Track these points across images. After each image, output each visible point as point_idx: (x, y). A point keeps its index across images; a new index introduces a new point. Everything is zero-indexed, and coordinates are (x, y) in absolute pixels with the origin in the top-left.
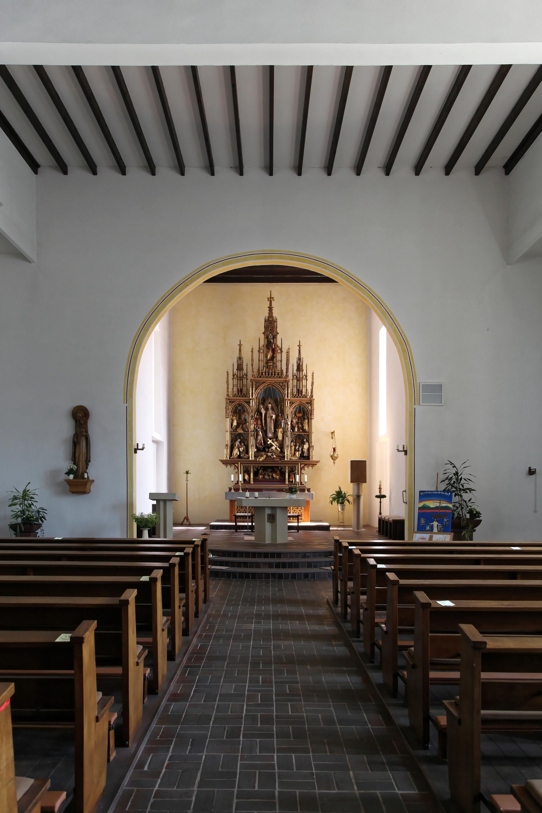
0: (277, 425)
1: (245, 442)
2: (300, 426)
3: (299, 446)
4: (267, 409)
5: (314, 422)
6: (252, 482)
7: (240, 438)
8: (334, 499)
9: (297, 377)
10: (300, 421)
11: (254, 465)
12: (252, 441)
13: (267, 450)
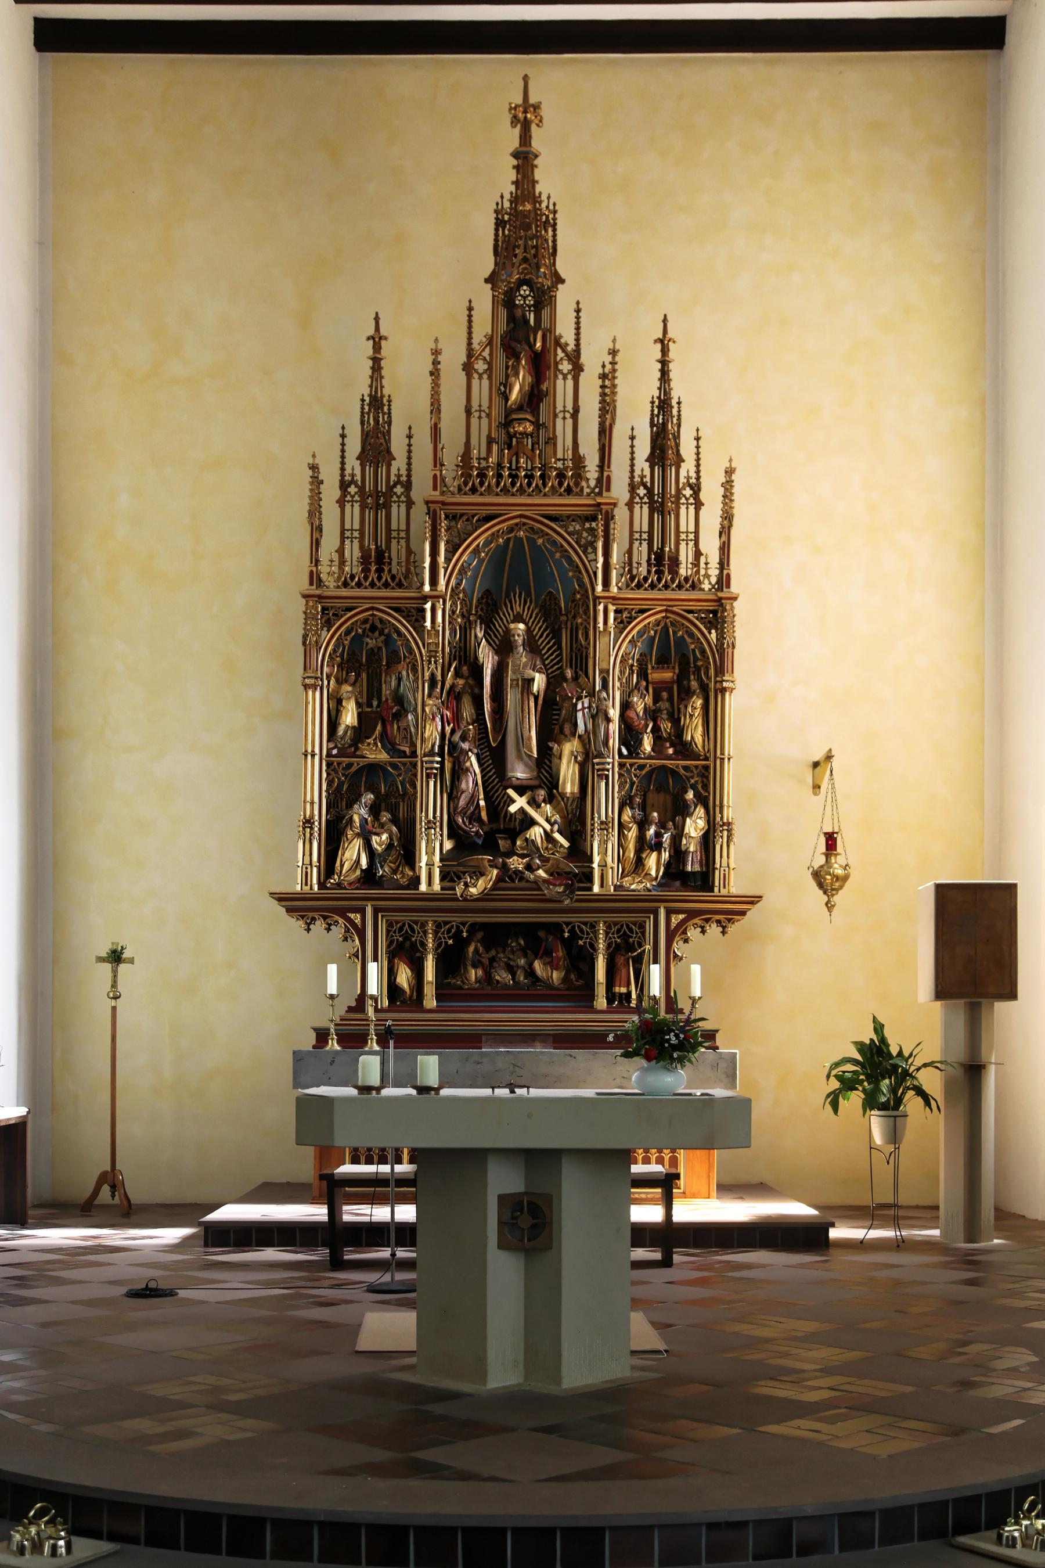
0: (554, 722)
1: (397, 808)
2: (666, 726)
3: (662, 825)
4: (504, 648)
5: (735, 706)
6: (430, 1001)
7: (371, 789)
8: (848, 1084)
9: (650, 491)
10: (664, 705)
11: (442, 918)
12: (431, 801)
13: (503, 844)
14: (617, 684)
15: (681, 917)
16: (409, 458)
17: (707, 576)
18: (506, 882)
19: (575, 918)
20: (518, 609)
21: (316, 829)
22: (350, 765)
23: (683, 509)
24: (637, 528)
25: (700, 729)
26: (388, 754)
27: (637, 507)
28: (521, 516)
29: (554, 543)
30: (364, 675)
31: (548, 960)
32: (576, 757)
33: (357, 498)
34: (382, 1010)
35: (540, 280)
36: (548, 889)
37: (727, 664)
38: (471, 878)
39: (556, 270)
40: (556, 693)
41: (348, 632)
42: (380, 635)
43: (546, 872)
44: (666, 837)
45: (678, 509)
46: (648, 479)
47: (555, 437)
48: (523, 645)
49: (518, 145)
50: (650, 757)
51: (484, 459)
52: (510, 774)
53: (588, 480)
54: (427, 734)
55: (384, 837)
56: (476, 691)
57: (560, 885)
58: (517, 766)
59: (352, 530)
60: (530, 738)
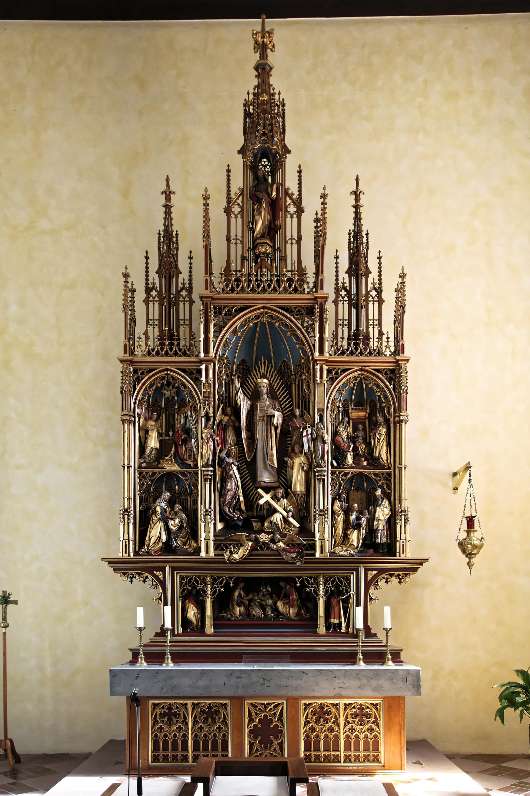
0: (288, 444)
1: (185, 501)
2: (362, 447)
3: (360, 512)
4: (254, 396)
5: (409, 432)
6: (210, 629)
7: (170, 489)
9: (349, 293)
10: (360, 434)
11: (216, 574)
12: (207, 498)
13: (256, 525)
14: (330, 419)
15: (374, 573)
16: (190, 272)
17: (388, 346)
18: (258, 550)
19: (304, 574)
20: (263, 371)
21: (132, 516)
22: (154, 474)
23: (371, 304)
24: (340, 317)
25: (385, 448)
26: (179, 466)
27: (340, 304)
28: (264, 307)
29: (286, 326)
30: (163, 415)
31: (286, 601)
32: (303, 467)
33: (157, 299)
34: (178, 635)
35: (275, 147)
36: (286, 555)
37: (403, 404)
38: (234, 548)
39: (284, 144)
40: (289, 426)
41: (151, 386)
42: (173, 388)
43: (284, 543)
44: (364, 520)
45: (367, 304)
46: (347, 285)
47: (286, 256)
48: (267, 393)
49: (259, 59)
50: (352, 468)
51: (239, 271)
52: (260, 479)
53: (308, 283)
54: (204, 452)
55: (177, 521)
56: (237, 424)
57: (294, 552)
58: (264, 474)
59: (154, 320)
60: (272, 455)
